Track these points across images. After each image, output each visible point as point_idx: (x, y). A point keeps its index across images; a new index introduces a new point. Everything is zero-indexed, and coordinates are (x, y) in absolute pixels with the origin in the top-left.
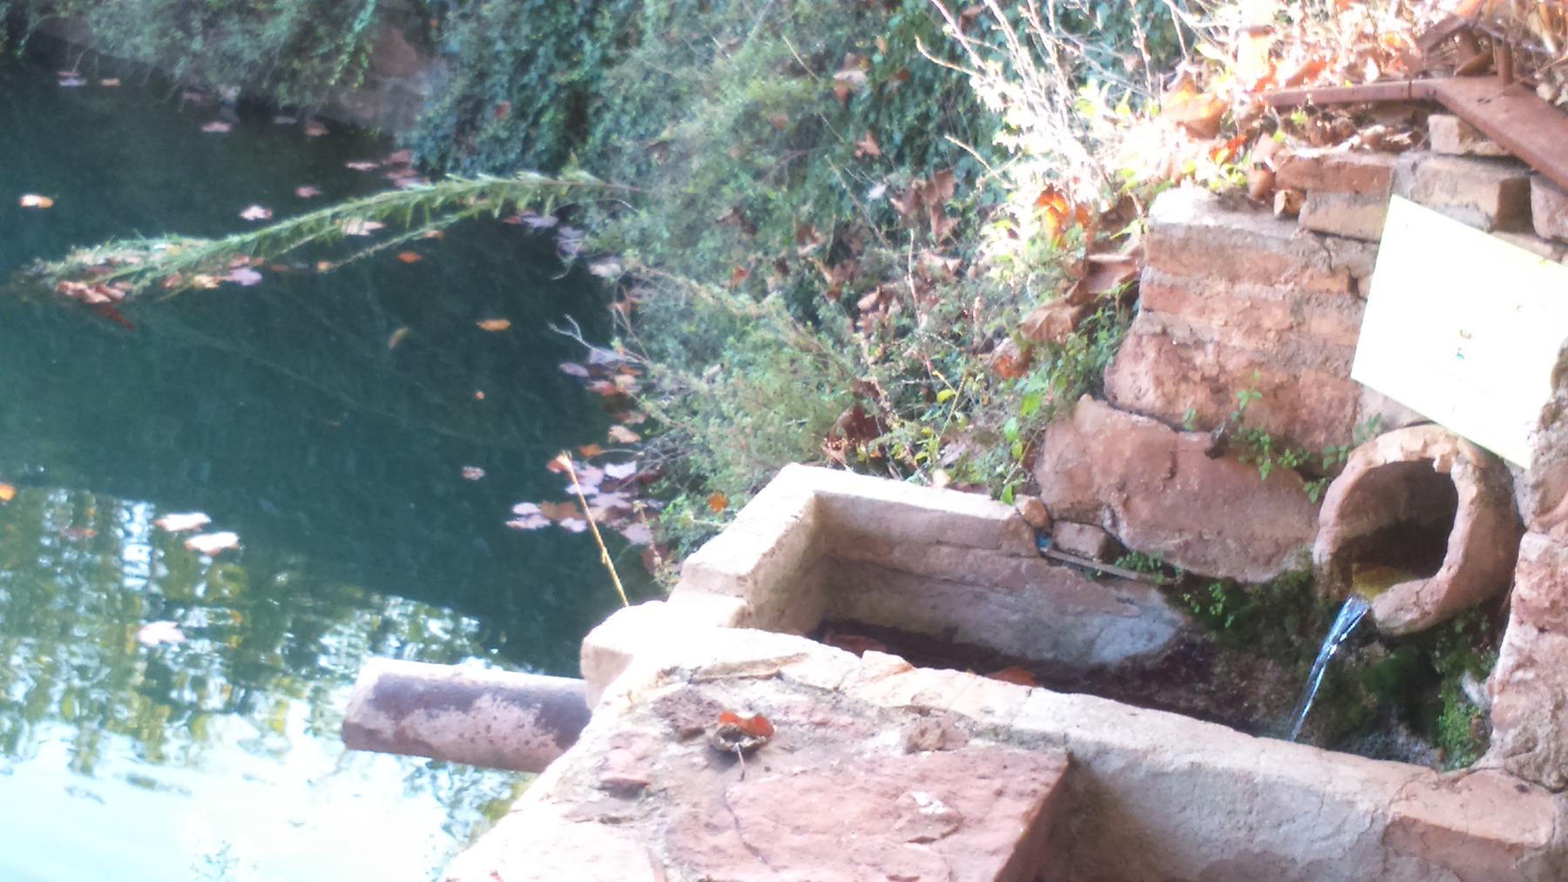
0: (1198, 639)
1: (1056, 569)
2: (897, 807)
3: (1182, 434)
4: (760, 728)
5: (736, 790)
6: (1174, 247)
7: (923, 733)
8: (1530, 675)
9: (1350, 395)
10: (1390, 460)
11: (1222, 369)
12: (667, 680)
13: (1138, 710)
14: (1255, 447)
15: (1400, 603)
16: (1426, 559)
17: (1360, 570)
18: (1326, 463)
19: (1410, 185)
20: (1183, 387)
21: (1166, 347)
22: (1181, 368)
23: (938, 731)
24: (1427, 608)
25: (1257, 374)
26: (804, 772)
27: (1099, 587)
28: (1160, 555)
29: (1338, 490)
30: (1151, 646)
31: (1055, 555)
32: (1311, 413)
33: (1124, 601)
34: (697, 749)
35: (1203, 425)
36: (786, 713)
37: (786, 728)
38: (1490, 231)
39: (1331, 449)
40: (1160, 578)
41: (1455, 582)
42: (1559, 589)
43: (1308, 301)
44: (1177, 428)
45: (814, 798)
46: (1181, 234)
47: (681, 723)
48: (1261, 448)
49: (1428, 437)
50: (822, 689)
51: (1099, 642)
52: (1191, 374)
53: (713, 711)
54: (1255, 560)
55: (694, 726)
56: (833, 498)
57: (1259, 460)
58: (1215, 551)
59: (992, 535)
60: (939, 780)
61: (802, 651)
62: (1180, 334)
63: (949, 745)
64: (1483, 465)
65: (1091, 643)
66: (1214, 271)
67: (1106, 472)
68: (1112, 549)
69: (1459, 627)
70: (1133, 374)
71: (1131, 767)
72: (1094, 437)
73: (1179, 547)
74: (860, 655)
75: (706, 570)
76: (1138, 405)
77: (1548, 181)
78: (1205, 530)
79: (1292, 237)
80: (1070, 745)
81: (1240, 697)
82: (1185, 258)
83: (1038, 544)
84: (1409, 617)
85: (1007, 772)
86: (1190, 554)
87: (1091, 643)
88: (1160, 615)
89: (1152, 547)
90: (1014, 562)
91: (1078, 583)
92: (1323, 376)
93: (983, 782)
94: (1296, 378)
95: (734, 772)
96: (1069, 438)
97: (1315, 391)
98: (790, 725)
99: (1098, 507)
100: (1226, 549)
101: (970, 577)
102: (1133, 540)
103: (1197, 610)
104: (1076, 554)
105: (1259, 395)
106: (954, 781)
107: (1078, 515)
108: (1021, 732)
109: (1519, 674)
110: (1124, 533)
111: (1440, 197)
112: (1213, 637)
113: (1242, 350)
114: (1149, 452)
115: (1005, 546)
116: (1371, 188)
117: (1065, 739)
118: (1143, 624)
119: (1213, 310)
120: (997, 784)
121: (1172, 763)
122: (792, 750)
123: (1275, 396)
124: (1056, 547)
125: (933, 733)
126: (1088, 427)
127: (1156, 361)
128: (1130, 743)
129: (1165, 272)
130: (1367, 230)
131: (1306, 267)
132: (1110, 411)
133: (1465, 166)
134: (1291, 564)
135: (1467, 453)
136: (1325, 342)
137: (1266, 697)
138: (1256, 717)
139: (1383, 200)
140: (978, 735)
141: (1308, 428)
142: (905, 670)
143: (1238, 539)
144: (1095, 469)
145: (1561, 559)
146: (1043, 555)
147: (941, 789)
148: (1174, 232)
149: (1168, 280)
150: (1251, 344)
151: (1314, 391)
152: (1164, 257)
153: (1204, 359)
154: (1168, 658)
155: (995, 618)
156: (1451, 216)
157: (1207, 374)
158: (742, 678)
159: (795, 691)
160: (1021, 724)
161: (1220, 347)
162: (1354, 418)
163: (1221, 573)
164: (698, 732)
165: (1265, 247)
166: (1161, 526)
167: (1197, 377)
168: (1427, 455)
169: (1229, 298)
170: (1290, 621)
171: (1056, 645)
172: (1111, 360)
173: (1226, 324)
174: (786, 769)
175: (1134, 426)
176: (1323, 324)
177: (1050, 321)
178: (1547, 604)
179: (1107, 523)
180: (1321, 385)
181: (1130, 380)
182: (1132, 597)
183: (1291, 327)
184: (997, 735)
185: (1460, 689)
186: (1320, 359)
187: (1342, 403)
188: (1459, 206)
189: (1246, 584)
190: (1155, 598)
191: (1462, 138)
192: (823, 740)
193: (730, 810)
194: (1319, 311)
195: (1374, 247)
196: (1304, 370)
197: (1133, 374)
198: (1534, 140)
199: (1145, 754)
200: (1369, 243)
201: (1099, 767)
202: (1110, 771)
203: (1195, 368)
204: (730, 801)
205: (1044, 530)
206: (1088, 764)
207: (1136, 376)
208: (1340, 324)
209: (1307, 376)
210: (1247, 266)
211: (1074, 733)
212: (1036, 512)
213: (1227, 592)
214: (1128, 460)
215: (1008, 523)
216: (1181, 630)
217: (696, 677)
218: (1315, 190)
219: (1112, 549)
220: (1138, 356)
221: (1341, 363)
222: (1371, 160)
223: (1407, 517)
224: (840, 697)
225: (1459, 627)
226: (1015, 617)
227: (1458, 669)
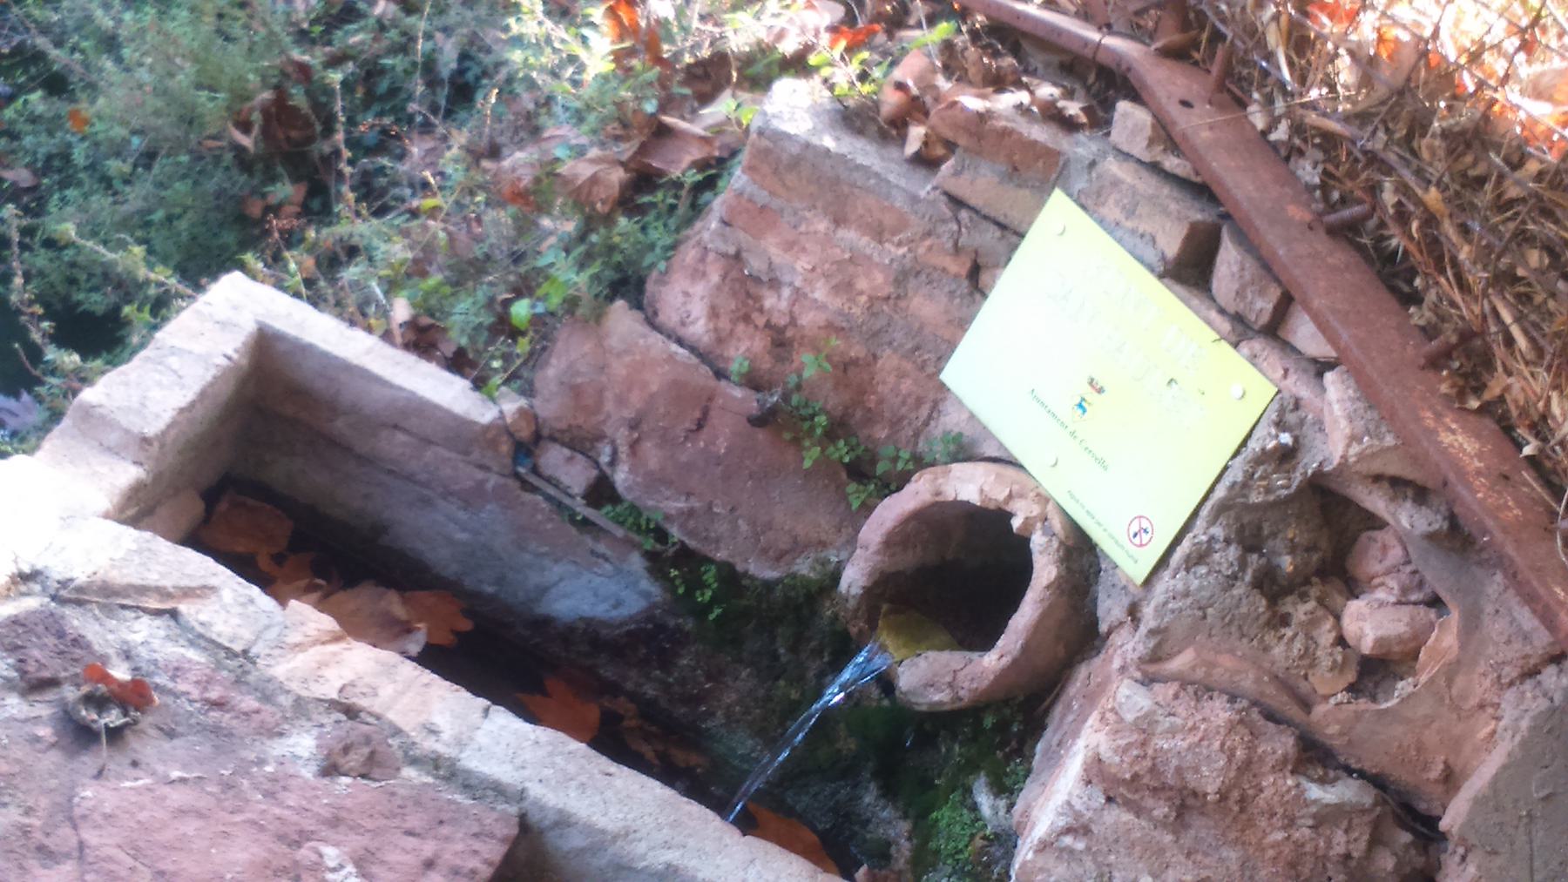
0: (672, 623)
1: (528, 497)
2: (296, 863)
3: (723, 383)
4: (135, 696)
5: (89, 793)
6: (783, 160)
7: (346, 750)
8: (1080, 845)
9: (931, 396)
10: (963, 497)
11: (793, 321)
12: (23, 588)
13: (614, 768)
14: (806, 425)
15: (933, 674)
16: (982, 635)
17: (890, 612)
18: (881, 468)
19: (1080, 184)
20: (741, 327)
21: (734, 274)
22: (745, 304)
23: (366, 750)
24: (962, 693)
25: (835, 342)
26: (183, 780)
27: (574, 531)
28: (659, 517)
29: (893, 510)
30: (614, 613)
31: (533, 479)
32: (881, 401)
33: (599, 556)
34: (44, 711)
35: (753, 382)
36: (173, 678)
37: (169, 700)
38: (1161, 277)
39: (889, 451)
40: (650, 544)
41: (1003, 675)
42: (1147, 763)
43: (918, 273)
44: (720, 374)
45: (190, 827)
46: (795, 150)
47: (31, 667)
48: (812, 429)
49: (1016, 488)
50: (227, 649)
51: (554, 591)
52: (755, 315)
53: (78, 652)
54: (764, 551)
55: (46, 674)
56: (278, 337)
57: (807, 443)
58: (722, 528)
59: (459, 434)
60: (355, 828)
61: (213, 582)
62: (755, 264)
63: (376, 773)
64: (1070, 543)
65: (543, 590)
66: (819, 204)
67: (621, 401)
68: (601, 491)
69: (989, 721)
70: (686, 294)
71: (596, 848)
72: (619, 355)
73: (681, 512)
74: (282, 602)
75: (102, 417)
76: (682, 332)
77: (1246, 241)
78: (718, 501)
79: (922, 194)
80: (525, 804)
81: (699, 699)
82: (791, 179)
83: (516, 461)
84: (937, 698)
85: (445, 830)
86: (691, 524)
87: (543, 590)
88: (636, 583)
89: (650, 503)
90: (480, 475)
91: (551, 520)
92: (908, 366)
93: (411, 842)
94: (875, 357)
95: (89, 761)
96: (588, 347)
97: (891, 379)
98: (176, 695)
99: (600, 437)
100: (735, 528)
101: (423, 477)
102: (629, 489)
103: (681, 591)
104: (556, 484)
105: (828, 366)
106: (375, 833)
107: (572, 440)
108: (468, 772)
109: (1068, 840)
110: (621, 477)
111: (1112, 211)
112: (689, 625)
113: (822, 307)
114: (678, 391)
115: (476, 455)
116: (1036, 170)
117: (521, 795)
118: (612, 587)
119: (804, 250)
120: (428, 848)
121: (643, 857)
122: (171, 734)
123: (845, 370)
124: (535, 470)
125: (361, 748)
126: (614, 342)
127: (718, 288)
128: (601, 822)
129: (762, 187)
130: (1014, 217)
131: (929, 234)
132: (646, 329)
133: (1148, 184)
134: (804, 567)
135: (1057, 524)
136: (921, 328)
137: (729, 707)
138: (710, 724)
139: (1042, 191)
140: (414, 761)
141: (871, 418)
142: (336, 639)
143: (752, 523)
144: (609, 395)
145: (1160, 729)
146: (517, 476)
147: (358, 841)
148: (787, 144)
149: (762, 197)
150: (837, 303)
151: (891, 375)
152: (765, 169)
153: (776, 303)
154: (629, 633)
155: (439, 531)
156: (1120, 241)
157: (774, 321)
158: (123, 607)
159: (192, 643)
160: (471, 761)
161: (798, 294)
162: (926, 424)
163: (721, 555)
164: (53, 683)
165: (888, 196)
166: (669, 483)
167: (760, 321)
168: (1008, 508)
169: (827, 241)
170: (784, 633)
171: (500, 580)
172: (662, 265)
173: (813, 269)
174: (160, 768)
175: (671, 358)
176: (926, 306)
177: (594, 180)
178: (1128, 776)
179: (604, 459)
180: (902, 375)
181: (680, 299)
182: (609, 553)
183: (888, 298)
184: (437, 768)
185: (968, 791)
186: (909, 346)
187: (919, 401)
188: (1133, 231)
189: (746, 574)
190: (636, 562)
191: (1151, 142)
192: (216, 730)
193: (75, 827)
194: (925, 290)
195: (1014, 239)
196: (888, 351)
197: (686, 294)
198: (1244, 183)
199: (615, 838)
200: (1012, 234)
201: (553, 839)
202: (566, 849)
203: (761, 310)
204: (77, 812)
205: (524, 446)
206: (541, 832)
207: (688, 298)
208: (946, 312)
209: (888, 360)
210: (860, 211)
211: (535, 790)
212: (523, 424)
213: (720, 578)
214: (652, 396)
215: (487, 428)
216: (654, 606)
217: (63, 593)
218: (966, 150)
219: (601, 491)
220: (698, 274)
221: (932, 356)
222: (1039, 133)
223: (969, 569)
224: (249, 666)
225: (989, 721)
226: (462, 536)
227: (972, 767)
